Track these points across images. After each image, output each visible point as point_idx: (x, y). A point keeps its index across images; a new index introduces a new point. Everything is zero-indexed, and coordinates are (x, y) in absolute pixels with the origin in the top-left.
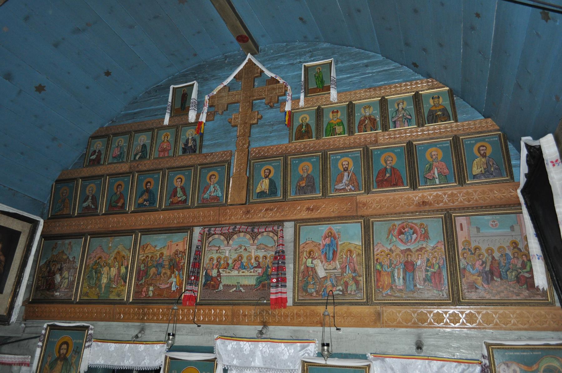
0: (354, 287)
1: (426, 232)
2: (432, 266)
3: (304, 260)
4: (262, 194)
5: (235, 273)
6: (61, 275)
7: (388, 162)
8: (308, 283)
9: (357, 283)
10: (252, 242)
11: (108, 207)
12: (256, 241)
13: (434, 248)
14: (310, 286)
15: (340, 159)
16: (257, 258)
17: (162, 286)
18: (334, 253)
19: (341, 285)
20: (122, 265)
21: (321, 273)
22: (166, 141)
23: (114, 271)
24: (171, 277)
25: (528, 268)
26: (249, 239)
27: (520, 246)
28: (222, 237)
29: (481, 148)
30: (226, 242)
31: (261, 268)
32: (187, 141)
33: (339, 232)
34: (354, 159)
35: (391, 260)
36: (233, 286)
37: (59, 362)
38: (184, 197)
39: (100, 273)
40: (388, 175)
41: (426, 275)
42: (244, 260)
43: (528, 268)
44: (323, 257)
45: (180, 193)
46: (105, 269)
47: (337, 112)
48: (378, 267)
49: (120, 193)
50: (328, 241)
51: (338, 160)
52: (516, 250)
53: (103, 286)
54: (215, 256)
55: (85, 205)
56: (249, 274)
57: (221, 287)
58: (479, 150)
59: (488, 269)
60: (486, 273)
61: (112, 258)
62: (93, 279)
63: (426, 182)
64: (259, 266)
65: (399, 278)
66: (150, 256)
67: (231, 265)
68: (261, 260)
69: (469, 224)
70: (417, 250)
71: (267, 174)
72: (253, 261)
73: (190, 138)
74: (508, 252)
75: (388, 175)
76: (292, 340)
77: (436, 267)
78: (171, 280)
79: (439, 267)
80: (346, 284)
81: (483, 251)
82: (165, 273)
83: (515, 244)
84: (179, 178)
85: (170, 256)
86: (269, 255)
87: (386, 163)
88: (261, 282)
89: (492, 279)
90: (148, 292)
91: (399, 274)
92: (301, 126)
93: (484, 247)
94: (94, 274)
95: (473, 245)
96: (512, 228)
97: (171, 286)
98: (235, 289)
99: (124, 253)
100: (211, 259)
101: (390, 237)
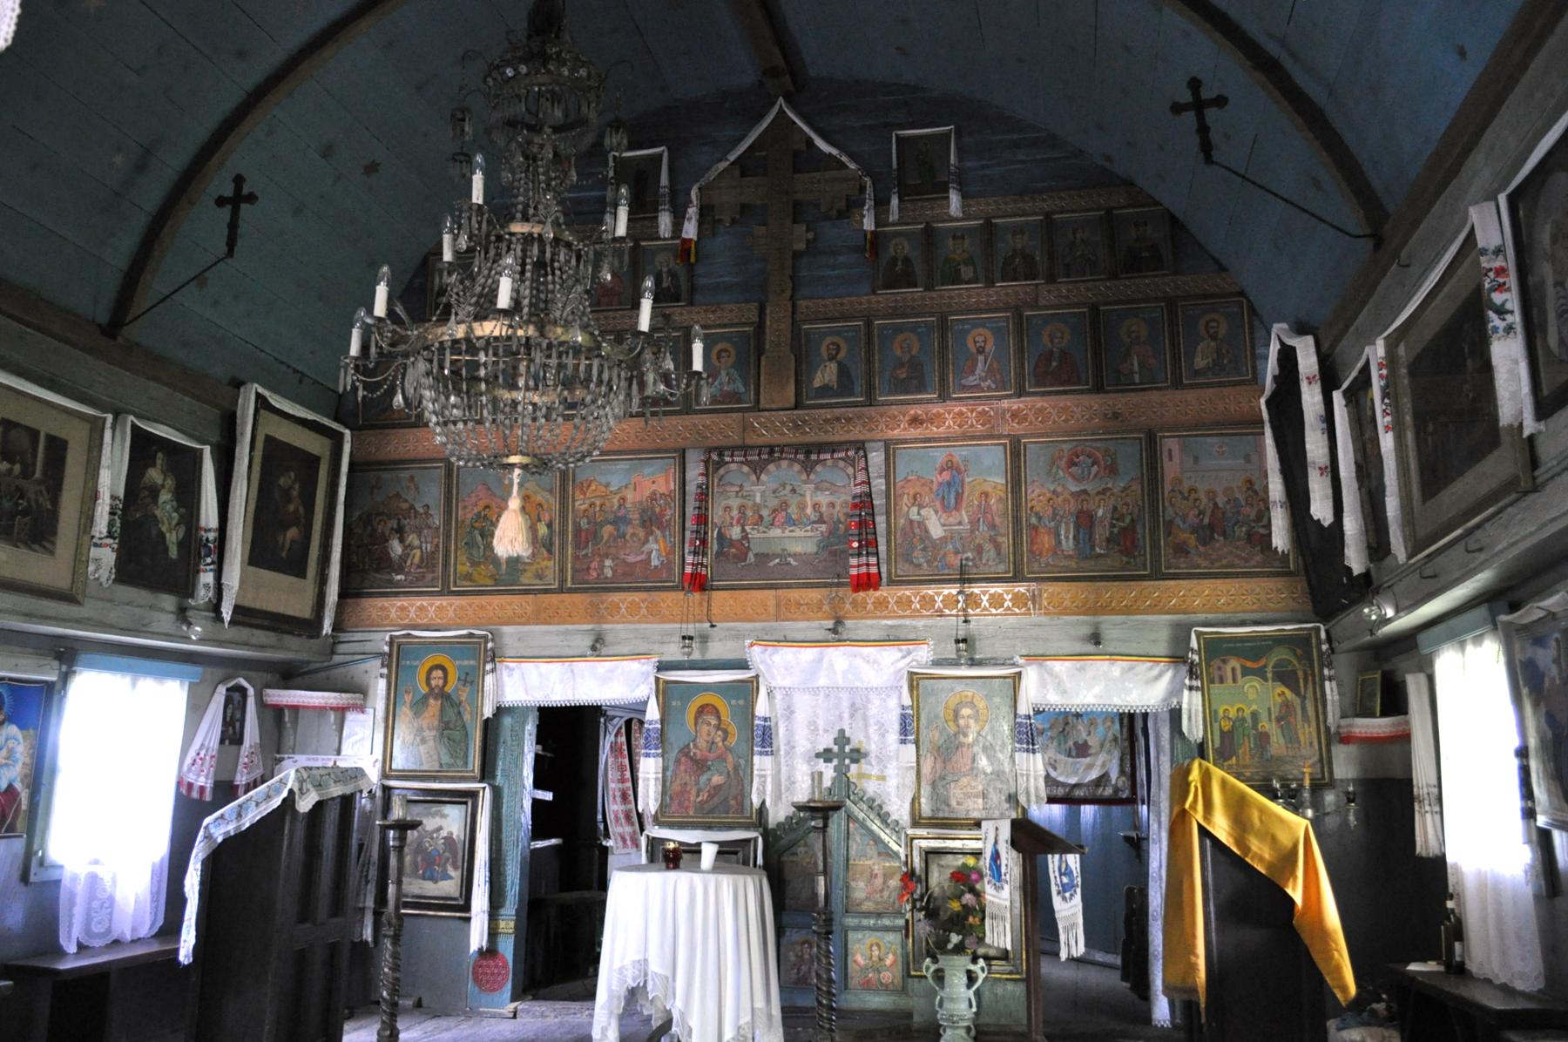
0: (993, 553)
1: (1114, 462)
2: (1121, 518)
4: (825, 390)
6: (402, 540)
8: (913, 548)
9: (997, 547)
10: (804, 477)
12: (812, 476)
13: (1125, 489)
15: (968, 331)
16: (816, 506)
17: (631, 559)
18: (959, 497)
21: (936, 531)
24: (646, 541)
25: (1265, 522)
28: (745, 469)
30: (754, 477)
34: (997, 332)
36: (776, 556)
37: (432, 701)
42: (793, 510)
43: (1265, 522)
44: (938, 504)
47: (963, 237)
48: (1034, 520)
50: (946, 476)
51: (965, 332)
54: (735, 503)
56: (802, 534)
57: (751, 558)
58: (1207, 326)
59: (1206, 521)
60: (1203, 528)
64: (821, 521)
65: (1067, 538)
67: (767, 519)
68: (824, 509)
70: (1098, 493)
72: (809, 511)
76: (891, 639)
77: (1128, 520)
78: (646, 548)
80: (979, 550)
81: (1202, 496)
82: (634, 535)
83: (1250, 483)
85: (641, 502)
89: (1212, 537)
91: (1067, 531)
92: (894, 261)
93: (1202, 488)
94: (479, 538)
95: (1186, 485)
96: (1247, 458)
99: (539, 498)
100: (728, 508)
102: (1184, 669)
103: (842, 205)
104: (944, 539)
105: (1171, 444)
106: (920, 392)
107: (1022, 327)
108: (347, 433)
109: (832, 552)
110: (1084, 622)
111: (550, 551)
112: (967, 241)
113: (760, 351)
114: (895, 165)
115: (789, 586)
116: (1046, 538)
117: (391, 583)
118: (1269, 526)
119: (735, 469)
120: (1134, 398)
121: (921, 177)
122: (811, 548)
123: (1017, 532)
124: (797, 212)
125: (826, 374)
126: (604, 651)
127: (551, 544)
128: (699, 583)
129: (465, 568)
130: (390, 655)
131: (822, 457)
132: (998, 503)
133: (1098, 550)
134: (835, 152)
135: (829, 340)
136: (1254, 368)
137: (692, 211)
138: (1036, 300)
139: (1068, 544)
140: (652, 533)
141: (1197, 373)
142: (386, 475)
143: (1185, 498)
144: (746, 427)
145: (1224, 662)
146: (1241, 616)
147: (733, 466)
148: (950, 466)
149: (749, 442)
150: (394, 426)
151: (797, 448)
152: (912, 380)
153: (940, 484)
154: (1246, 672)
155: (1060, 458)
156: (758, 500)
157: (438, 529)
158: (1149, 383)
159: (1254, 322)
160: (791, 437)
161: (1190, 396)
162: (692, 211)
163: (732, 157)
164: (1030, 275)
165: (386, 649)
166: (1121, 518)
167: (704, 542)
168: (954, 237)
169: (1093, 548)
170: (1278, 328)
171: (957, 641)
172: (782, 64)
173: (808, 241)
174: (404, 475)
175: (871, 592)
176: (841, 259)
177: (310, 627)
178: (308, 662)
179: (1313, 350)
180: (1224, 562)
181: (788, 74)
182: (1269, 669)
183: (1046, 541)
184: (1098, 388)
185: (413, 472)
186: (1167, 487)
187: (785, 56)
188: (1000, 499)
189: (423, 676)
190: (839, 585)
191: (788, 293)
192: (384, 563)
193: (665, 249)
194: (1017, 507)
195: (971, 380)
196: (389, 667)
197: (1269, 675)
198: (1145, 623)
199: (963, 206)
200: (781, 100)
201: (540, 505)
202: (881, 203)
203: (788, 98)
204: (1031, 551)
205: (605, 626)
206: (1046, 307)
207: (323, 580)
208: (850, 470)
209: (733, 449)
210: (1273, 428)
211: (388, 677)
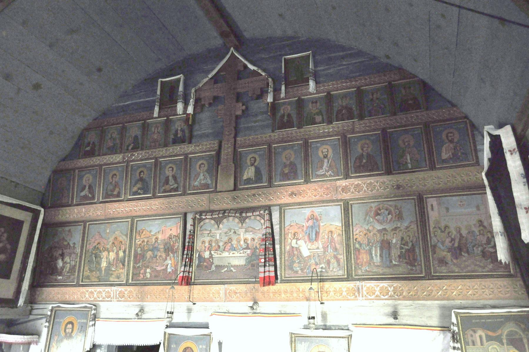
0: (336, 264)
2: (406, 244)
3: (289, 241)
4: (249, 181)
5: (226, 254)
6: (63, 260)
7: (365, 149)
8: (294, 262)
9: (338, 261)
10: (240, 225)
11: (104, 195)
12: (244, 225)
13: (407, 227)
14: (296, 265)
16: (245, 240)
17: (159, 268)
18: (317, 234)
19: (324, 263)
20: (120, 250)
21: (306, 253)
22: (156, 132)
23: (112, 255)
24: (166, 259)
26: (238, 223)
27: (485, 224)
28: (213, 222)
29: (450, 135)
30: (216, 226)
31: (249, 249)
32: (177, 131)
33: (320, 214)
35: (368, 239)
36: (224, 267)
38: (176, 185)
39: (100, 257)
40: (364, 161)
41: (401, 252)
42: (234, 242)
43: (492, 243)
44: (306, 238)
45: (171, 181)
46: (104, 254)
47: (316, 102)
48: (357, 246)
49: (115, 182)
50: (310, 223)
51: (317, 148)
52: (482, 228)
53: (103, 269)
54: (207, 239)
55: (83, 194)
56: (239, 255)
57: (213, 268)
58: (447, 136)
59: (456, 245)
61: (111, 243)
62: (93, 263)
63: (399, 167)
64: (247, 248)
65: (376, 255)
66: (146, 240)
67: (222, 247)
68: (249, 242)
69: (439, 204)
70: (393, 230)
71: (253, 162)
72: (242, 242)
73: (179, 129)
74: (474, 229)
75: (364, 161)
77: (410, 244)
79: (413, 245)
80: (328, 263)
82: (161, 256)
84: (170, 167)
85: (164, 240)
86: (257, 237)
87: (362, 150)
88: (250, 262)
90: (145, 274)
91: (376, 251)
92: (283, 116)
93: (452, 226)
94: (94, 258)
95: (442, 225)
96: (478, 208)
97: (167, 268)
98: (226, 269)
99: (121, 239)
101: (368, 218)
102: (449, 335)
103: (259, 93)
104: (309, 257)
105: (432, 202)
106: (294, 179)
107: (346, 143)
108: (42, 210)
109: (252, 263)
110: (389, 305)
111: (124, 265)
112: (318, 104)
113: (218, 163)
114: (283, 72)
115: (231, 283)
116: (365, 256)
117: (56, 280)
118: (495, 246)
119: (208, 223)
120: (408, 177)
121: (296, 76)
122: (242, 262)
123: (348, 252)
124: (239, 97)
125: (249, 173)
126: (144, 316)
127: (124, 261)
128: (187, 281)
129: (87, 273)
130: (51, 316)
131: (248, 214)
132: (338, 238)
133: (394, 262)
134: (255, 68)
135: (251, 156)
136: (477, 158)
137: (192, 102)
138: (354, 130)
139: (377, 259)
140: (169, 255)
141: (444, 161)
142: (60, 229)
143: (442, 232)
144: (210, 201)
145: (475, 332)
146: (482, 302)
147: (207, 221)
148: (312, 217)
149: (212, 208)
150: (58, 207)
151: (236, 210)
152: (291, 174)
153: (307, 227)
154: (489, 338)
155: (371, 211)
156: (218, 238)
157: (77, 254)
158: (416, 168)
159: (473, 130)
160: (235, 205)
161: (440, 173)
162: (192, 102)
163: (210, 76)
164: (351, 117)
165: (49, 313)
166: (406, 244)
167: (191, 260)
168: (313, 103)
169: (391, 262)
170: (489, 129)
171: (309, 318)
172: (228, 30)
173: (243, 111)
174: (67, 229)
175: (271, 287)
176: (260, 118)
177: (12, 303)
178: (20, 319)
179: (511, 133)
180: (469, 268)
181: (231, 33)
182: (504, 337)
183: (364, 257)
184: (389, 172)
185: (70, 227)
186: (432, 225)
187: (227, 22)
188: (339, 234)
189: (64, 327)
190: (255, 282)
191: (233, 135)
192: (54, 271)
193: (179, 120)
194: (348, 238)
195: (321, 172)
196: (49, 322)
197: (505, 341)
198: (424, 305)
199: (316, 87)
200: (232, 49)
201: (121, 242)
202: (277, 91)
203: (237, 49)
204: (357, 264)
205: (145, 303)
206: (359, 132)
207: (21, 280)
208: (262, 221)
209: (206, 212)
210: (492, 189)
211: (48, 327)
